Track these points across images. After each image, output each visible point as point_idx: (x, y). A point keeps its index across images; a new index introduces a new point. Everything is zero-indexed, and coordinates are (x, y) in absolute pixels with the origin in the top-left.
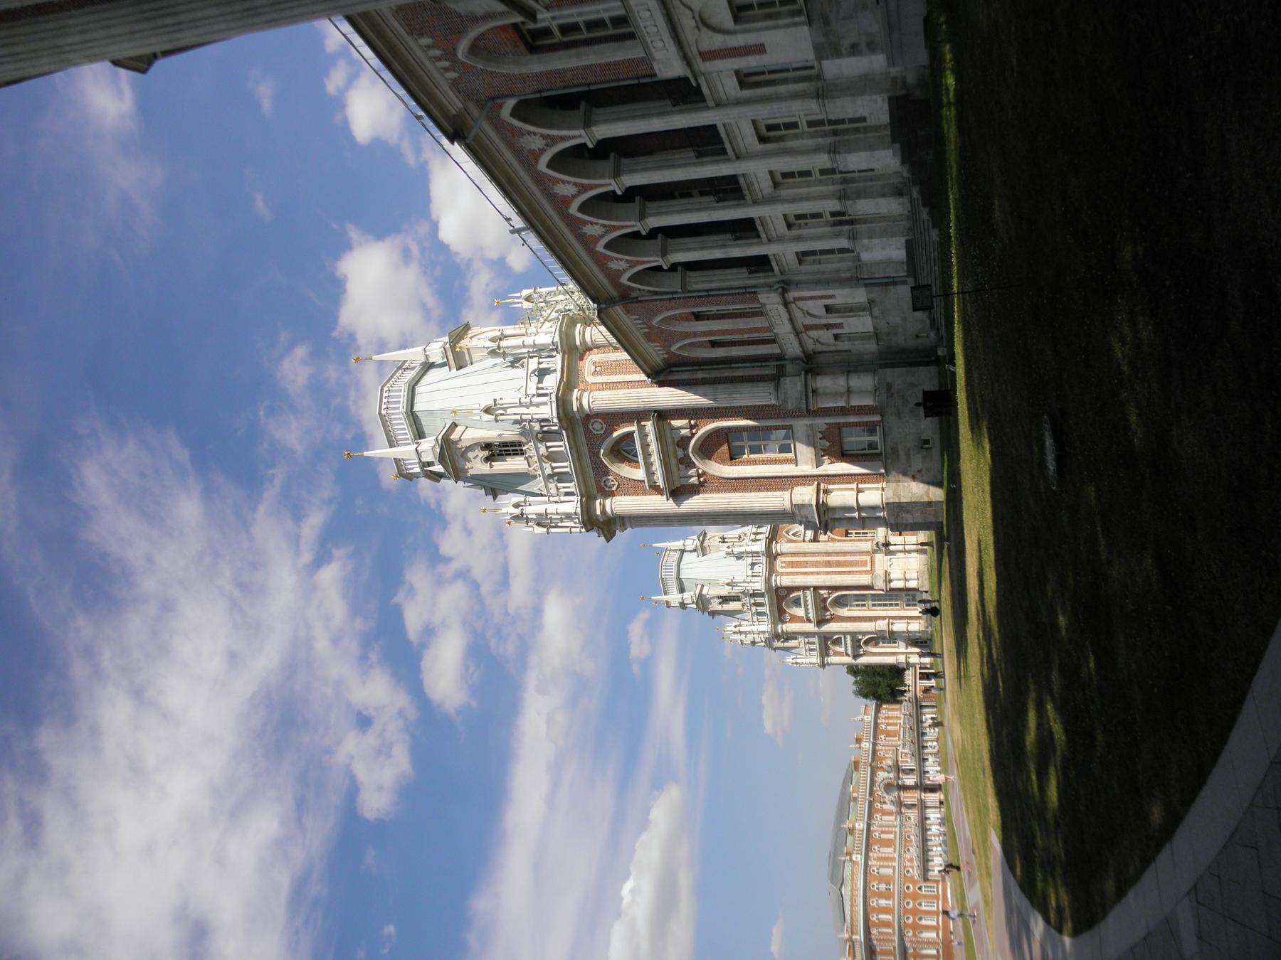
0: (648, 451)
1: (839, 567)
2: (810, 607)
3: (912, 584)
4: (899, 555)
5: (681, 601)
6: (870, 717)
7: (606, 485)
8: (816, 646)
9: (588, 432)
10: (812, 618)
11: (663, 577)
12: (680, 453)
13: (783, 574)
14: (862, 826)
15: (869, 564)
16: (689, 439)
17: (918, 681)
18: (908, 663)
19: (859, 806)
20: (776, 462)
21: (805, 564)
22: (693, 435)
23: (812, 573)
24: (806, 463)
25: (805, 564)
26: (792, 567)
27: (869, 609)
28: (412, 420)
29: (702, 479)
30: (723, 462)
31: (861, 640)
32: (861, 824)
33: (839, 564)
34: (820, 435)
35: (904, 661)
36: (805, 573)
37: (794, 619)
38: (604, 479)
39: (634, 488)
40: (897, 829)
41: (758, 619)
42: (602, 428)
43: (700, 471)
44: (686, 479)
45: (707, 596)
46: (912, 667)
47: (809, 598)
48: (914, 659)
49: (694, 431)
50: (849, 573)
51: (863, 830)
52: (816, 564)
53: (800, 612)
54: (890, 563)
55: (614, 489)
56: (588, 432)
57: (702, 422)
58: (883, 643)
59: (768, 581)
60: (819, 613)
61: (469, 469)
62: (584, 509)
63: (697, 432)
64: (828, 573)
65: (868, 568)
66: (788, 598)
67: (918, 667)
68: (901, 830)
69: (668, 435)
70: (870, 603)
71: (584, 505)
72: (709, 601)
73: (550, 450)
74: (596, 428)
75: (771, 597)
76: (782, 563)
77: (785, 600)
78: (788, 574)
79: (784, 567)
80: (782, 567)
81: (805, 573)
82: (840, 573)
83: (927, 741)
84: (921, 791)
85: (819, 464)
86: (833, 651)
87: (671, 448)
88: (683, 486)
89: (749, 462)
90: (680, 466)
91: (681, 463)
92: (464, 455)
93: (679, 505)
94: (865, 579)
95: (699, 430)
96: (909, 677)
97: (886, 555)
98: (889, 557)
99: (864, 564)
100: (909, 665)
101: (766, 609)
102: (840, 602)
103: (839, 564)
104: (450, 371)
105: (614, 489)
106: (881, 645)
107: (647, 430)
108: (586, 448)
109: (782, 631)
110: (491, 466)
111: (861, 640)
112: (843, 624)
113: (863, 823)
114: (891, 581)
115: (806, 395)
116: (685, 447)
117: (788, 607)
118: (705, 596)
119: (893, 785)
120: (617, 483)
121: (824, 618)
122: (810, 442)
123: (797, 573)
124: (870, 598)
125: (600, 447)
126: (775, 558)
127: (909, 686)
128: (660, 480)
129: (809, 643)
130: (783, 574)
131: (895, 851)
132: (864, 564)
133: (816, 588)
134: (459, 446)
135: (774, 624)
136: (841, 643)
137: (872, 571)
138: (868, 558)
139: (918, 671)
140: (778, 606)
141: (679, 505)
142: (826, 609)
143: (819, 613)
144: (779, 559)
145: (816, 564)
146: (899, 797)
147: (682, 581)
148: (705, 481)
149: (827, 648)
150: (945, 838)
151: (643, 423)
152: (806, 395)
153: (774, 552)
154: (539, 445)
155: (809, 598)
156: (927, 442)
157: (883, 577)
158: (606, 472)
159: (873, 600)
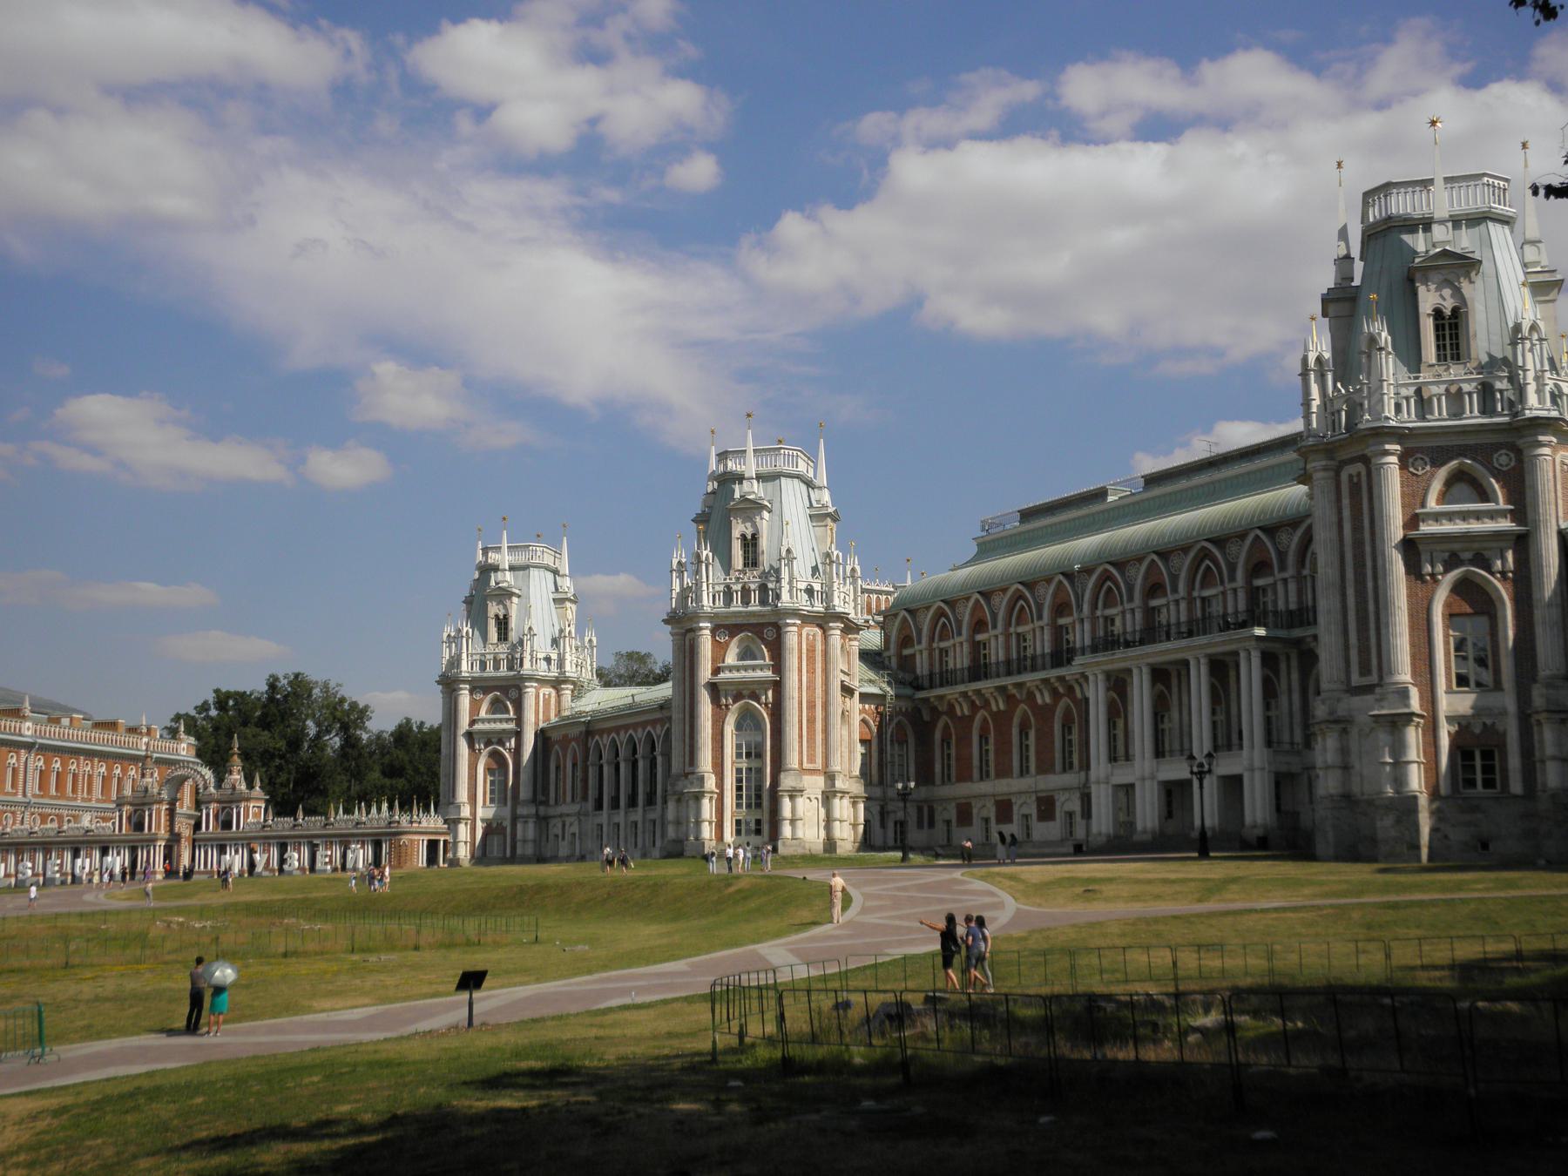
0: (1470, 518)
1: (808, 720)
2: (743, 674)
3: (786, 831)
4: (822, 811)
5: (746, 476)
6: (184, 753)
7: (1416, 459)
8: (490, 671)
9: (1496, 447)
10: (722, 675)
11: (782, 451)
12: (1467, 555)
13: (800, 635)
14: (27, 733)
15: (811, 766)
16: (1489, 569)
17: (426, 838)
18: (457, 821)
19: (13, 724)
20: (1448, 668)
21: (811, 671)
22: (1492, 574)
23: (800, 680)
24: (1449, 704)
25: (811, 671)
26: (807, 650)
27: (733, 763)
28: (1477, 216)
29: (1428, 578)
30: (1447, 605)
31: (503, 745)
32: (30, 733)
33: (811, 721)
34: (1489, 722)
35: (462, 815)
36: (800, 670)
37: (720, 650)
38: (1427, 459)
39: (1414, 496)
40: (20, 798)
41: (719, 592)
42: (1501, 465)
43: (1440, 577)
44: (1429, 558)
45: (758, 518)
46: (449, 828)
47: (759, 674)
48: (463, 832)
49: (1498, 575)
50: (801, 736)
51: (21, 735)
52: (812, 687)
53: (731, 659)
54: (812, 797)
55: (1411, 469)
56: (1496, 447)
57: (1509, 585)
58: (492, 783)
59: (795, 613)
60: (732, 688)
61: (1427, 286)
62: (1397, 430)
63: (1496, 578)
64: (800, 703)
65: (806, 765)
66: (759, 641)
67: (450, 838)
68: (17, 804)
69: (1494, 545)
70: (744, 766)
71: (1400, 431)
72: (751, 520)
73: (1467, 397)
74: (1504, 463)
75: (763, 615)
76: (814, 636)
77: (755, 637)
78: (800, 643)
79: (807, 639)
80: (808, 635)
81: (800, 670)
82: (800, 722)
83: (33, 860)
84: (168, 840)
85: (1450, 719)
86: (482, 700)
87: (1476, 545)
88: (1418, 554)
89: (1446, 636)
90: (1447, 554)
91: (1450, 556)
92: (1448, 283)
93: (1396, 547)
94: (792, 759)
95: (1499, 581)
96: (432, 822)
97: (823, 792)
98: (820, 797)
99: (812, 759)
100: (452, 824)
101: (737, 606)
102: (748, 721)
103: (811, 721)
104: (1345, 226)
105: (1411, 469)
106: (489, 778)
107: (1500, 520)
108: (1472, 442)
109: (701, 629)
110: (1429, 315)
111: (503, 745)
112: (710, 722)
113: (31, 737)
114: (792, 798)
115: (1560, 712)
116: (1473, 562)
117: (741, 641)
118: (760, 513)
119: (177, 791)
120: (1420, 473)
121: (722, 693)
122: (1478, 710)
123: (800, 658)
124: (755, 764)
125: (1473, 459)
126: (820, 626)
127: (420, 823)
128: (1426, 528)
129: (495, 660)
130: (800, 635)
131: (34, 796)
132: (812, 759)
133: (778, 686)
134: (1462, 279)
135: (711, 617)
136: (493, 713)
137: (803, 771)
138: (819, 764)
139: (442, 838)
140: (744, 625)
141: (1396, 547)
142: (736, 699)
143: (732, 688)
144: (818, 631)
145: (812, 687)
146: (160, 802)
147: (774, 480)
148: (1424, 582)
149: (486, 690)
150: (58, 882)
151: (1509, 516)
152: (1560, 712)
153: (831, 624)
154: (1474, 384)
155: (759, 674)
156: (1485, 846)
157: (799, 786)
158: (1437, 463)
159: (749, 770)
